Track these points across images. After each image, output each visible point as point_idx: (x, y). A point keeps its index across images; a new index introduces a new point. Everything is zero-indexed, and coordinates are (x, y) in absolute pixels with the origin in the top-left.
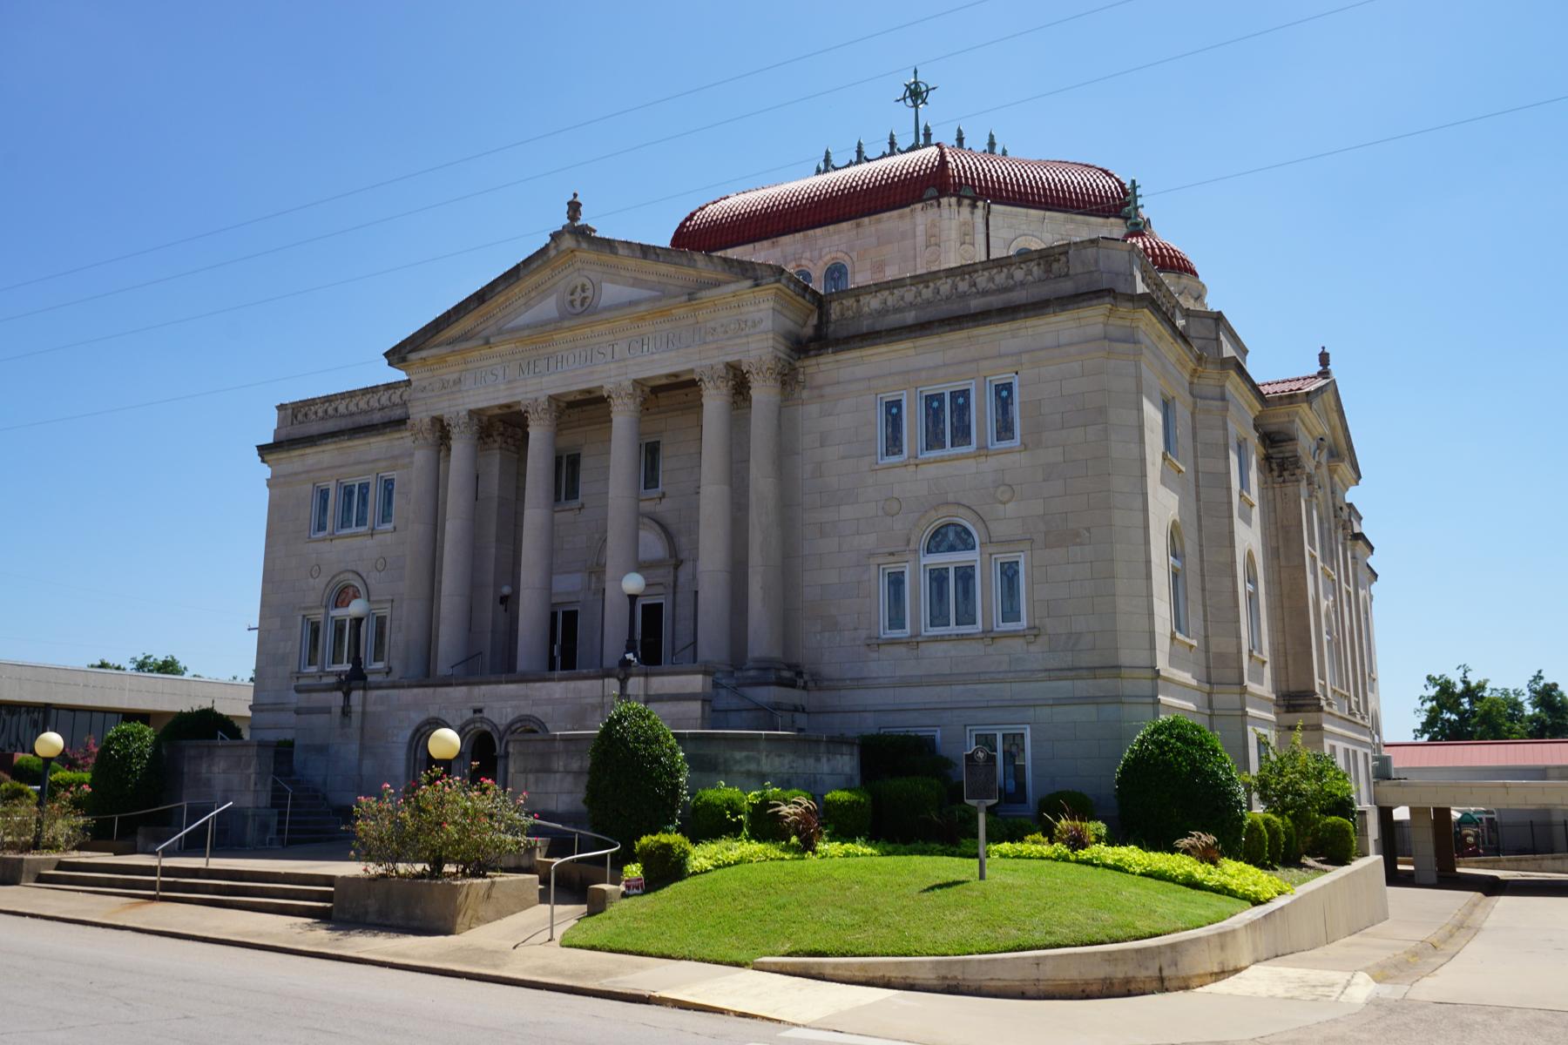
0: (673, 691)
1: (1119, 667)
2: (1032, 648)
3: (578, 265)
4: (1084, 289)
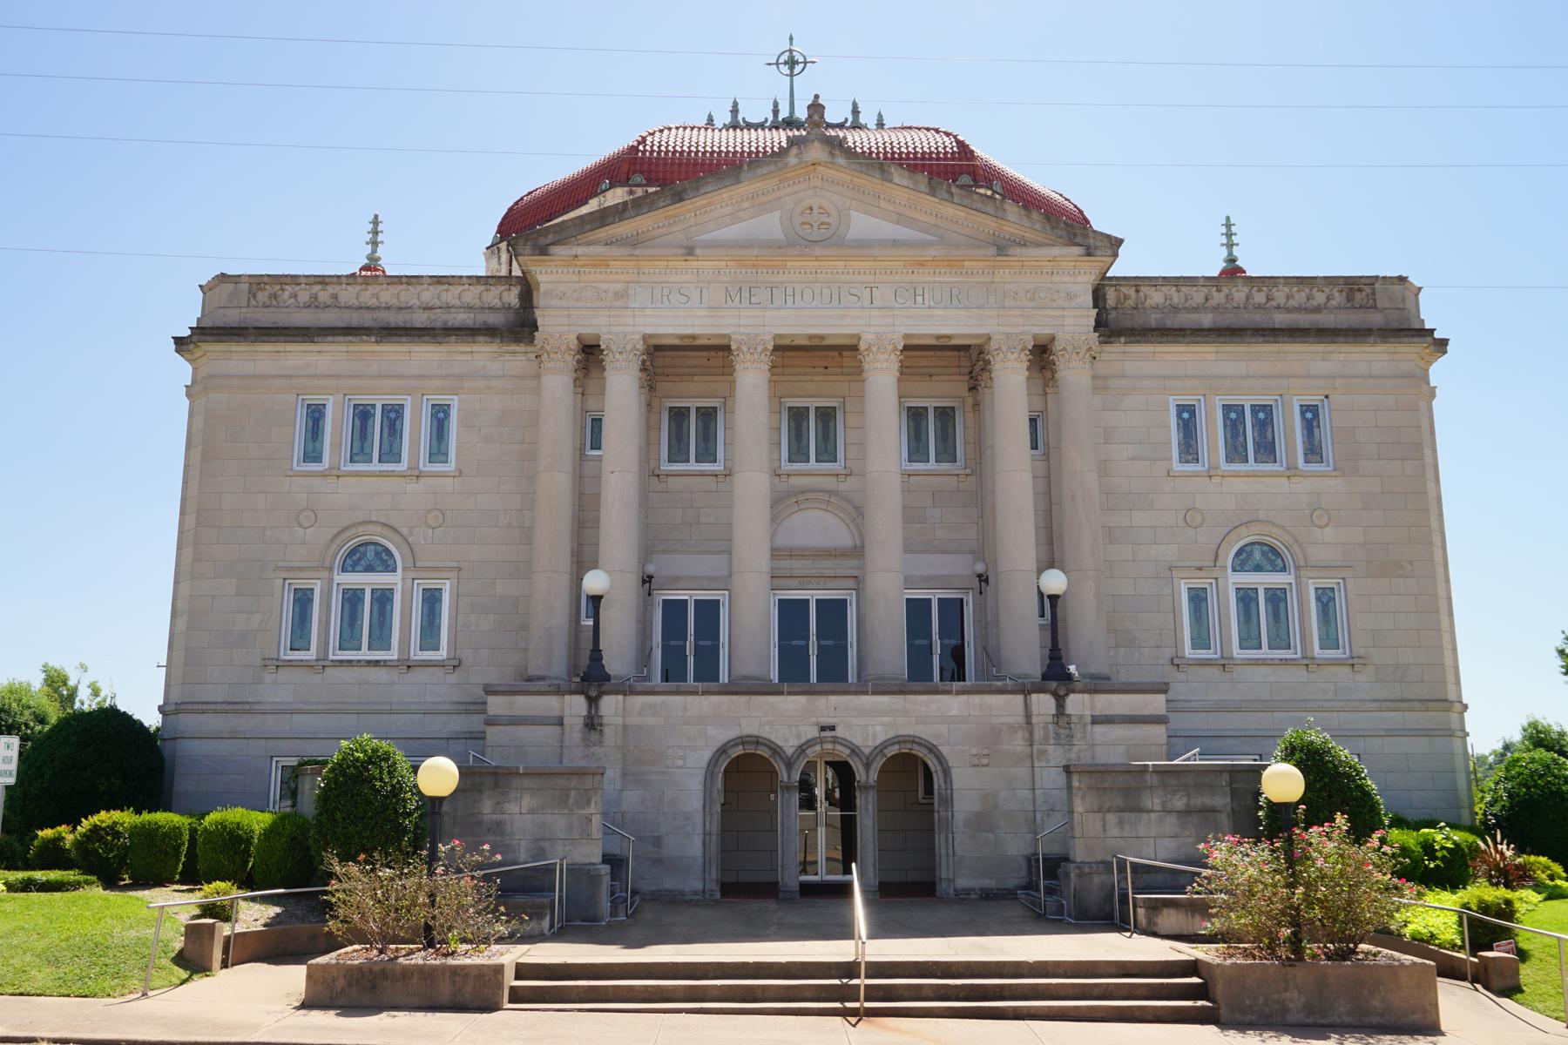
2: (1359, 677)
3: (816, 182)
4: (1394, 325)
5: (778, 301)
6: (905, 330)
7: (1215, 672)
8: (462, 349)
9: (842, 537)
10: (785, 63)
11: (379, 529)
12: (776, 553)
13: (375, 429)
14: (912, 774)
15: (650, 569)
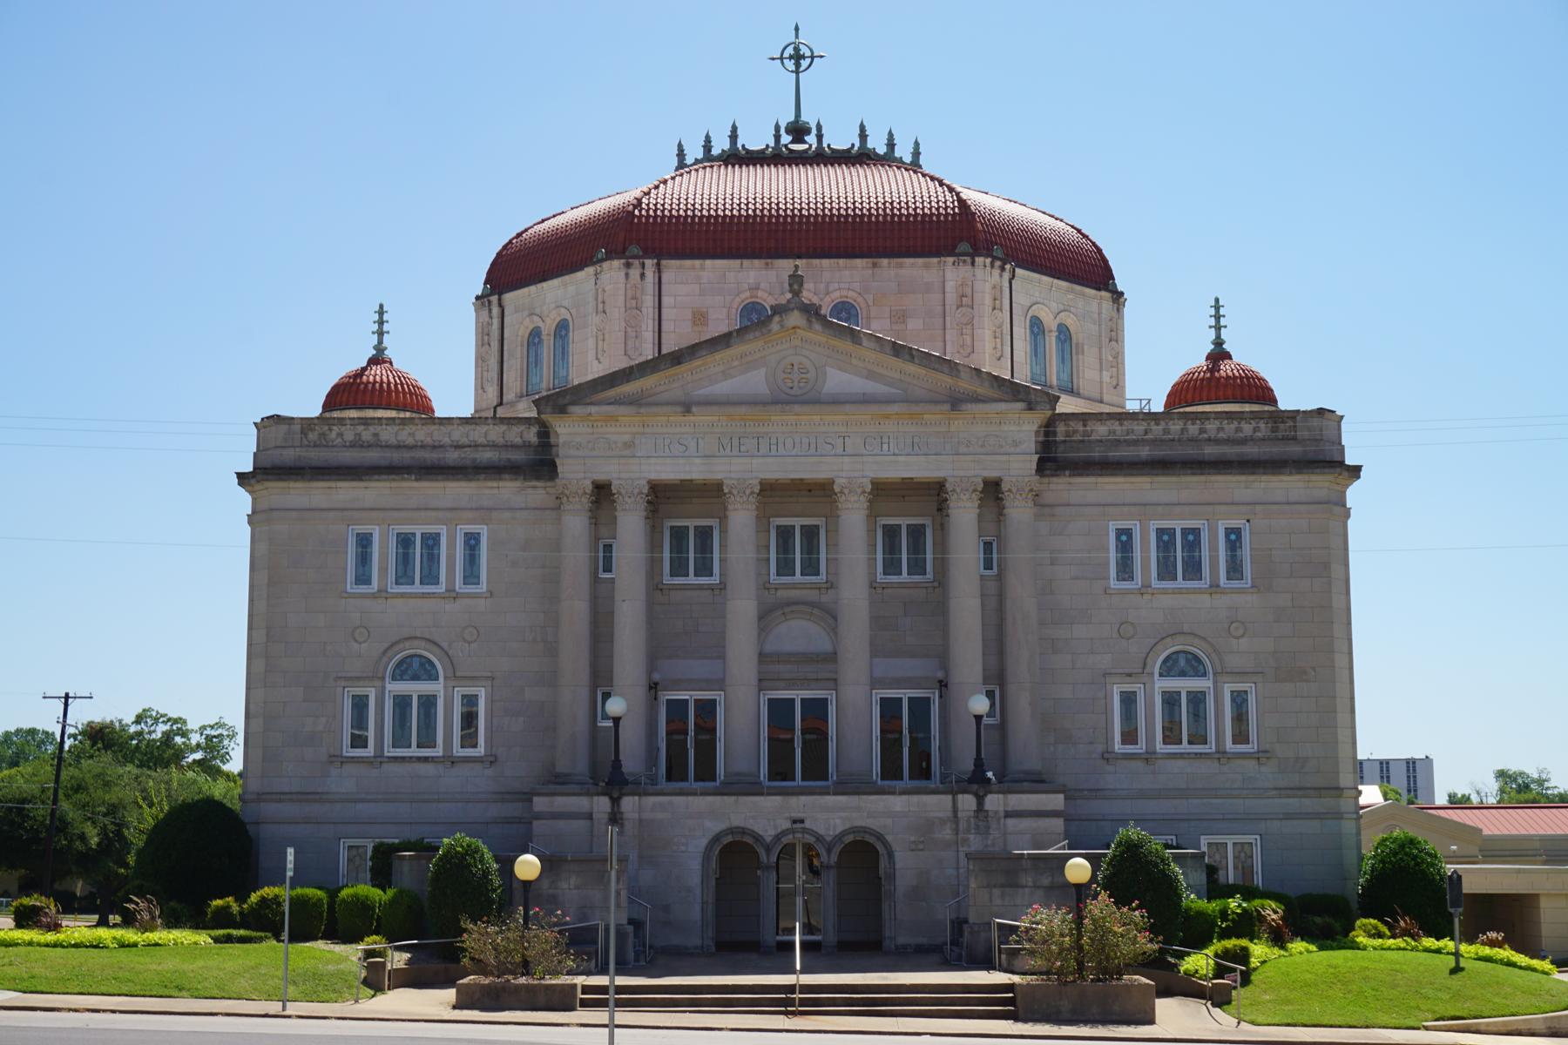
0: (1032, 808)
1: (1338, 788)
2: (1263, 769)
5: (763, 450)
6: (872, 475)
7: (1140, 764)
8: (490, 484)
9: (824, 645)
10: (791, 57)
11: (423, 643)
12: (763, 657)
13: (414, 557)
14: (862, 857)
15: (656, 677)
